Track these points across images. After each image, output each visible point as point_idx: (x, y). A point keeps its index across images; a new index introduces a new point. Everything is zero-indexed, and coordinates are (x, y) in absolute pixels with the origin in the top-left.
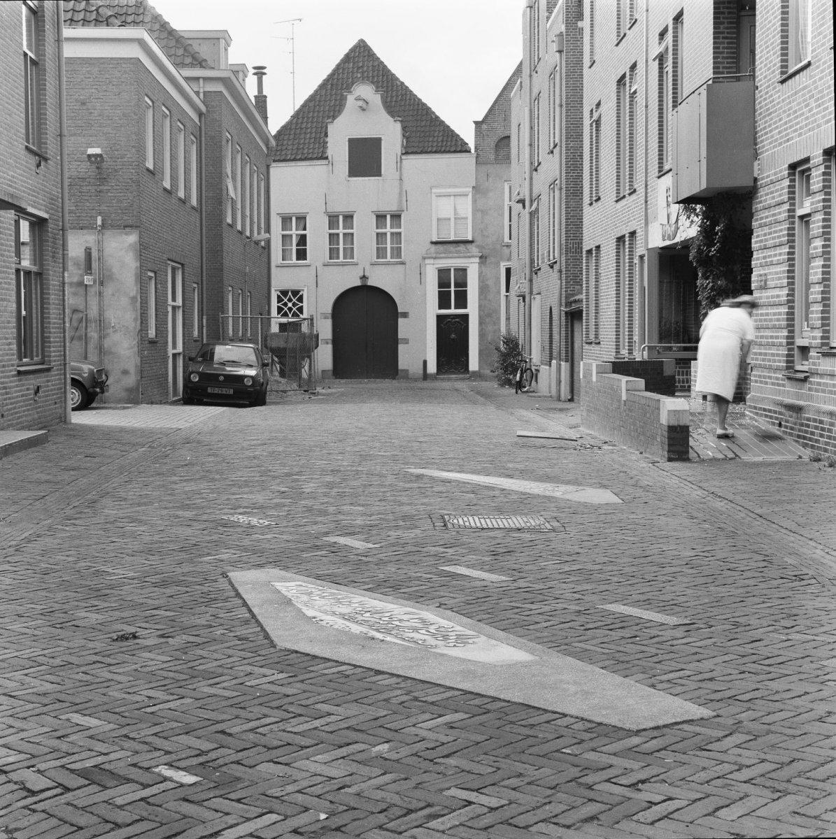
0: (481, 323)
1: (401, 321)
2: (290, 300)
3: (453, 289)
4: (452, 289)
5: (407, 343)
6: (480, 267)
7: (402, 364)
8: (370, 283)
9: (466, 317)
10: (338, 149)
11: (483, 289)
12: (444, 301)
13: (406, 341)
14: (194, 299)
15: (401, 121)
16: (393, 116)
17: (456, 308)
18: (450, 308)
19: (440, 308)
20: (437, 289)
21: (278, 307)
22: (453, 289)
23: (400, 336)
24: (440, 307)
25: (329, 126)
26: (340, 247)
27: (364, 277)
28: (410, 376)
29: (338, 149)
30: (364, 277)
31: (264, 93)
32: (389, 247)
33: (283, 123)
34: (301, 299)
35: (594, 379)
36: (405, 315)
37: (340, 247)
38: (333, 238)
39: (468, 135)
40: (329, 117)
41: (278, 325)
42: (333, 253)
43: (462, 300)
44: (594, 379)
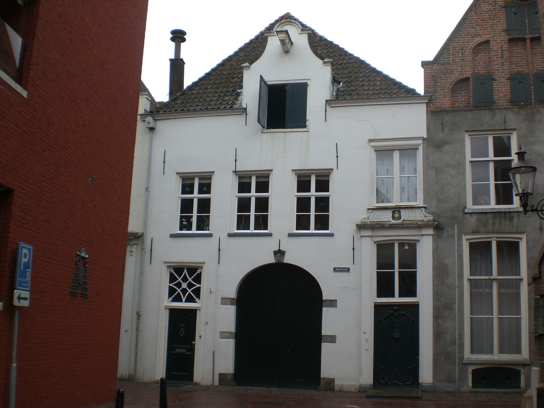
0: (437, 316)
1: (326, 311)
2: (185, 279)
3: (397, 270)
4: (394, 272)
5: (334, 342)
6: (435, 241)
7: (327, 369)
8: (287, 260)
9: (416, 306)
10: (250, 93)
11: (440, 271)
12: (384, 286)
13: (332, 339)
14: (491, 294)
15: (333, 65)
16: (322, 58)
17: (400, 296)
18: (393, 296)
19: (471, 275)
20: (295, 213)
21: (170, 287)
22: (397, 270)
23: (326, 331)
24: (379, 295)
25: (244, 72)
26: (253, 213)
27: (279, 253)
28: (336, 388)
29: (250, 93)
30: (279, 253)
31: (173, 44)
32: (313, 213)
33: (196, 79)
34: (198, 279)
35: (24, 93)
36: (333, 303)
37: (253, 213)
38: (243, 205)
39: (421, 90)
40: (245, 61)
41: (168, 311)
42: (243, 222)
43: (409, 285)
44: (24, 93)
